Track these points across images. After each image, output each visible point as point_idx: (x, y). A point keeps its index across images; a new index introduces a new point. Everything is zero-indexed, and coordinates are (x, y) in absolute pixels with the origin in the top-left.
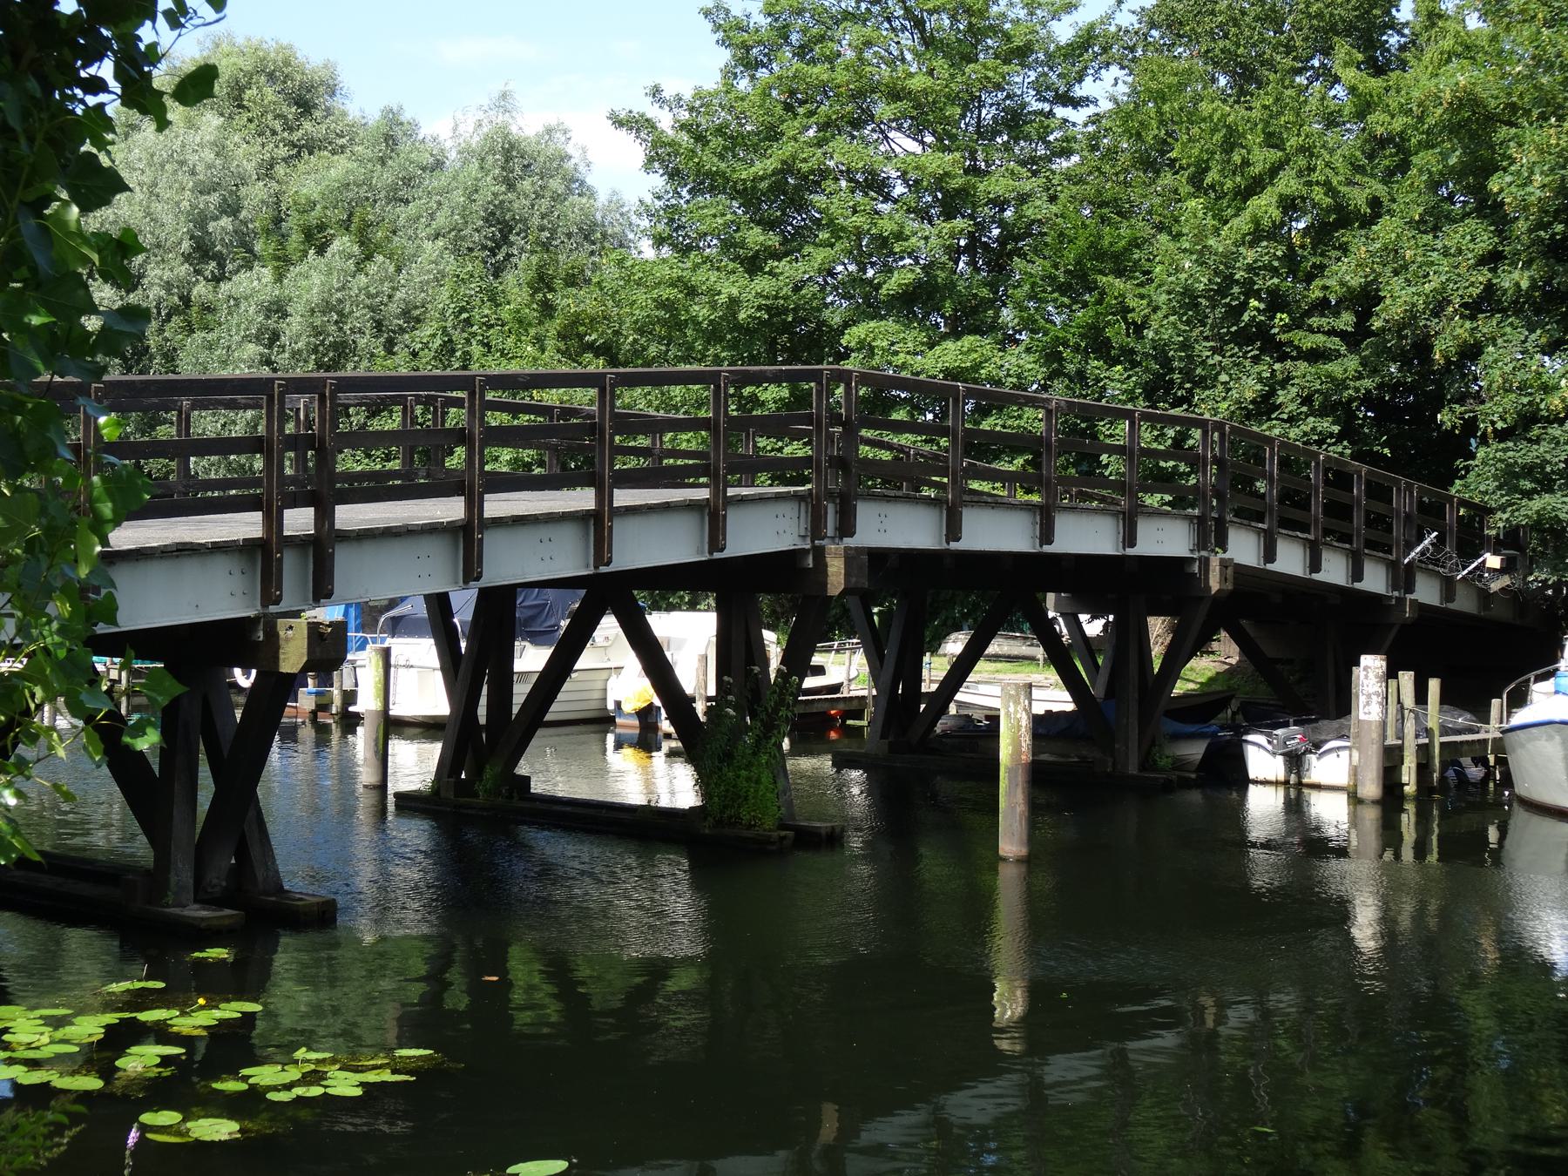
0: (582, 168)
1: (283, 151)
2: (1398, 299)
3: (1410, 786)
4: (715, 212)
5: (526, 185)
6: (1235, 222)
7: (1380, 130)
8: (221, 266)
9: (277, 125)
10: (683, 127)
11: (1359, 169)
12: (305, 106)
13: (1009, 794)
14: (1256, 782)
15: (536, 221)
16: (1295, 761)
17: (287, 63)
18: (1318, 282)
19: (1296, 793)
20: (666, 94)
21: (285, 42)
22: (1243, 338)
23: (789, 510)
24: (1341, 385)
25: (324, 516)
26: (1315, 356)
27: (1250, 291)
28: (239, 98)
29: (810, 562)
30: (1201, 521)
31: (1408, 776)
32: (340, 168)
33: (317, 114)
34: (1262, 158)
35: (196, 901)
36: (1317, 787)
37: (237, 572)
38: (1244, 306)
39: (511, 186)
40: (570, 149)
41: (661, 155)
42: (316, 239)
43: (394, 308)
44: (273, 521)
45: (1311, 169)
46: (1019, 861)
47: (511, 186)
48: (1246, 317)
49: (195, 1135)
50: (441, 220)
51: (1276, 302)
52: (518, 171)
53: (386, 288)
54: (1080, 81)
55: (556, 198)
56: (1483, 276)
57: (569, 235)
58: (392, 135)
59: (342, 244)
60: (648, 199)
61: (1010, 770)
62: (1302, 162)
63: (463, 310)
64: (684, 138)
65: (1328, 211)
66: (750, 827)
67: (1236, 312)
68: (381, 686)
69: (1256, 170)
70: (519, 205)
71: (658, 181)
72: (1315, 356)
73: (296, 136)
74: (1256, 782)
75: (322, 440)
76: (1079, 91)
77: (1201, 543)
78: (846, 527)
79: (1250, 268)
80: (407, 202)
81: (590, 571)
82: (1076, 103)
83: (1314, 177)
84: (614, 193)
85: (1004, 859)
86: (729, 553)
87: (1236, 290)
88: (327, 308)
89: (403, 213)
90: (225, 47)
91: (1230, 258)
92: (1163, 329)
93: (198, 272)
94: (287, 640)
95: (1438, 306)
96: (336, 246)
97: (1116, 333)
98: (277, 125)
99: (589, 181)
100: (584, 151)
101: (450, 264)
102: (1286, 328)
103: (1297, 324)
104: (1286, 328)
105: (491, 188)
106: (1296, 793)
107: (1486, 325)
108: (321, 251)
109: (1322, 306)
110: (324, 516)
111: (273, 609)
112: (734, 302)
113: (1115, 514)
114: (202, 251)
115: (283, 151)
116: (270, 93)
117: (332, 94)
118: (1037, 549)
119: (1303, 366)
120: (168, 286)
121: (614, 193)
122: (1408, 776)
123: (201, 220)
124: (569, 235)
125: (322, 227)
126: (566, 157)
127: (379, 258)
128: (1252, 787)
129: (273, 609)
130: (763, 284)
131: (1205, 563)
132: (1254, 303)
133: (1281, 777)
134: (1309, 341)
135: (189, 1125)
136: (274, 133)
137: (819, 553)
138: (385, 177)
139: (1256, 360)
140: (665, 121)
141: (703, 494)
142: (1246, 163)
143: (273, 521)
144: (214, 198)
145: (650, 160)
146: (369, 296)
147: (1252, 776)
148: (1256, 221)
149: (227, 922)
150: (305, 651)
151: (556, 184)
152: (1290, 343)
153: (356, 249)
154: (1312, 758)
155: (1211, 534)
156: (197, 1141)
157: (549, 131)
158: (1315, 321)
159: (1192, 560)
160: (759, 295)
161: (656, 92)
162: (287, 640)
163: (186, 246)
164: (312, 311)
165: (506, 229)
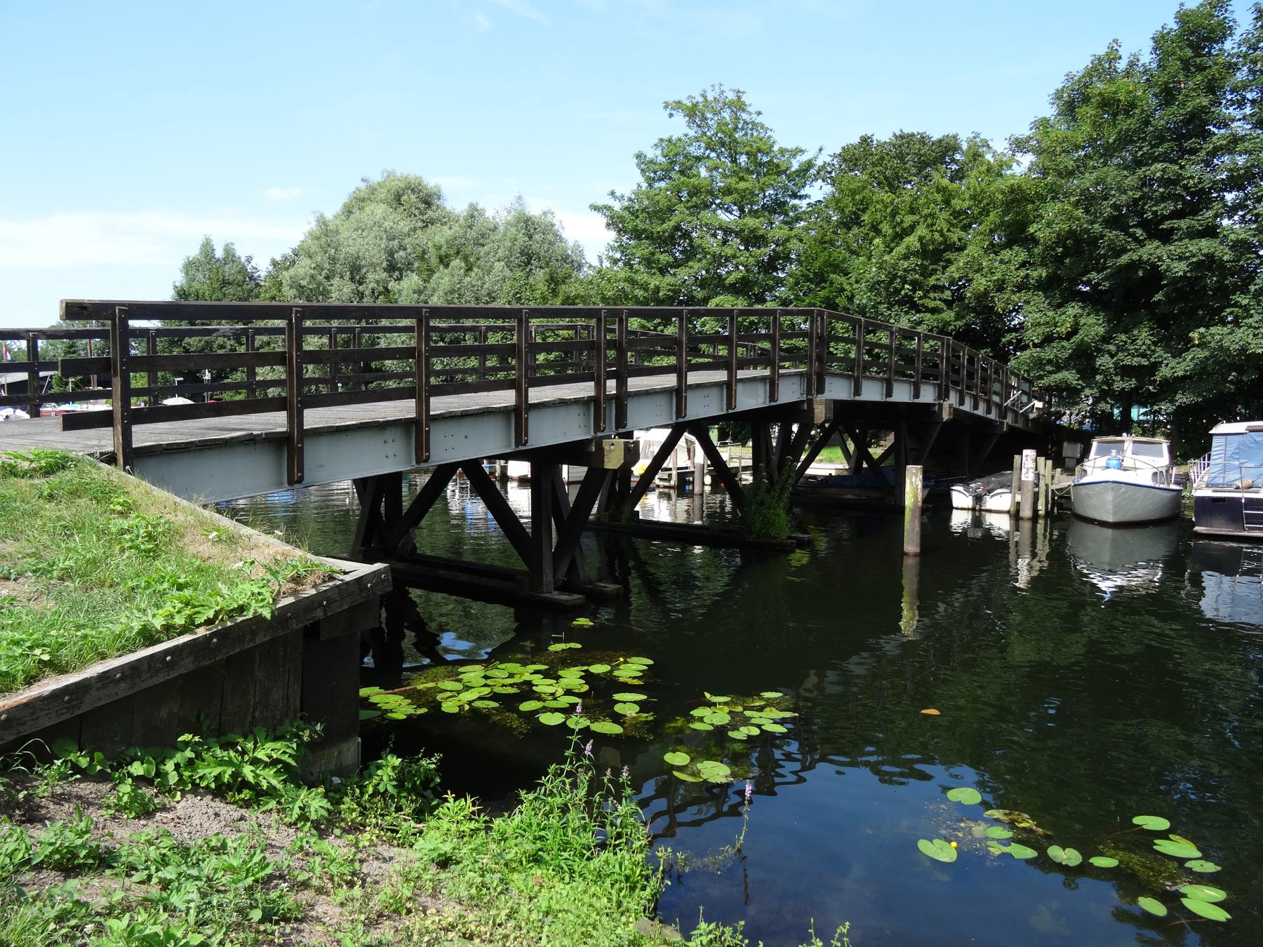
0: (561, 230)
1: (420, 224)
2: (981, 283)
3: (1042, 513)
4: (645, 248)
5: (537, 237)
6: (898, 249)
7: (958, 208)
8: (401, 274)
9: (417, 212)
10: (627, 208)
11: (953, 225)
12: (428, 204)
13: (912, 521)
14: (957, 509)
15: (542, 253)
16: (978, 499)
17: (420, 185)
18: (934, 277)
19: (978, 512)
20: (618, 194)
21: (418, 175)
22: (901, 303)
23: (796, 380)
24: (948, 323)
25: (622, 384)
26: (934, 311)
27: (904, 281)
28: (399, 200)
29: (805, 407)
30: (940, 386)
31: (1041, 507)
32: (448, 233)
33: (434, 208)
34: (909, 220)
35: (556, 589)
36: (990, 511)
37: (582, 414)
38: (903, 288)
39: (530, 237)
40: (555, 222)
41: (615, 222)
42: (444, 261)
43: (484, 292)
44: (600, 386)
45: (933, 225)
46: (915, 555)
47: (530, 237)
48: (903, 293)
49: (705, 777)
50: (500, 253)
51: (916, 285)
52: (532, 231)
53: (479, 283)
54: (803, 187)
55: (551, 243)
56: (1022, 273)
57: (557, 260)
58: (474, 214)
59: (457, 263)
60: (612, 243)
61: (913, 511)
62: (929, 221)
63: (517, 293)
64: (626, 214)
65: (941, 243)
66: (774, 538)
67: (897, 291)
68: (1138, 530)
69: (905, 225)
70: (535, 247)
71: (612, 235)
72: (934, 311)
73: (425, 217)
74: (957, 509)
75: (620, 343)
76: (802, 192)
77: (939, 397)
78: (821, 390)
79: (905, 270)
80: (483, 245)
81: (724, 412)
82: (801, 197)
83: (934, 228)
84: (576, 241)
85: (907, 554)
86: (779, 402)
87: (898, 280)
88: (452, 292)
89: (483, 250)
90: (392, 178)
91: (894, 267)
92: (862, 299)
93: (391, 276)
94: (610, 451)
95: (1000, 287)
96: (453, 264)
97: (841, 301)
98: (417, 212)
99: (564, 236)
100: (561, 222)
101: (508, 273)
102: (921, 298)
103: (925, 296)
104: (921, 298)
105: (522, 239)
106: (978, 512)
107: (1023, 296)
108: (447, 266)
109: (935, 288)
110: (622, 384)
111: (599, 434)
112: (657, 289)
113: (910, 383)
114: (392, 268)
115: (420, 224)
116: (413, 198)
117: (439, 199)
118: (884, 400)
119: (928, 315)
120: (378, 282)
121: (576, 241)
122: (1041, 507)
123: (391, 253)
124: (557, 260)
125: (447, 256)
126: (553, 225)
127: (475, 269)
128: (954, 511)
129: (599, 434)
130: (669, 279)
131: (941, 406)
132: (907, 286)
133: (970, 506)
134: (931, 304)
135: (699, 766)
136: (415, 216)
137: (810, 402)
138: (472, 234)
139: (907, 313)
140: (617, 206)
141: (767, 372)
142: (902, 221)
143: (600, 386)
144: (396, 242)
145: (608, 225)
146: (473, 286)
147: (955, 505)
148: (908, 248)
149: (578, 601)
150: (622, 457)
151: (550, 237)
152: (923, 305)
153: (463, 265)
154: (988, 498)
155: (943, 394)
156: (705, 781)
157: (545, 214)
158: (932, 295)
159: (935, 404)
160: (668, 284)
161: (613, 193)
162: (610, 451)
163: (385, 264)
164: (446, 294)
165: (530, 258)
